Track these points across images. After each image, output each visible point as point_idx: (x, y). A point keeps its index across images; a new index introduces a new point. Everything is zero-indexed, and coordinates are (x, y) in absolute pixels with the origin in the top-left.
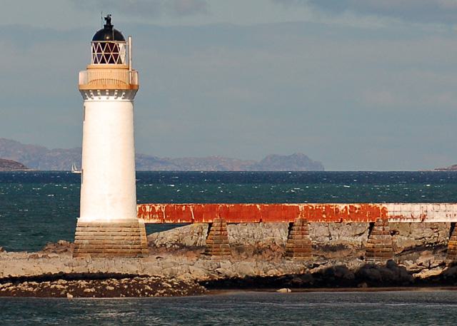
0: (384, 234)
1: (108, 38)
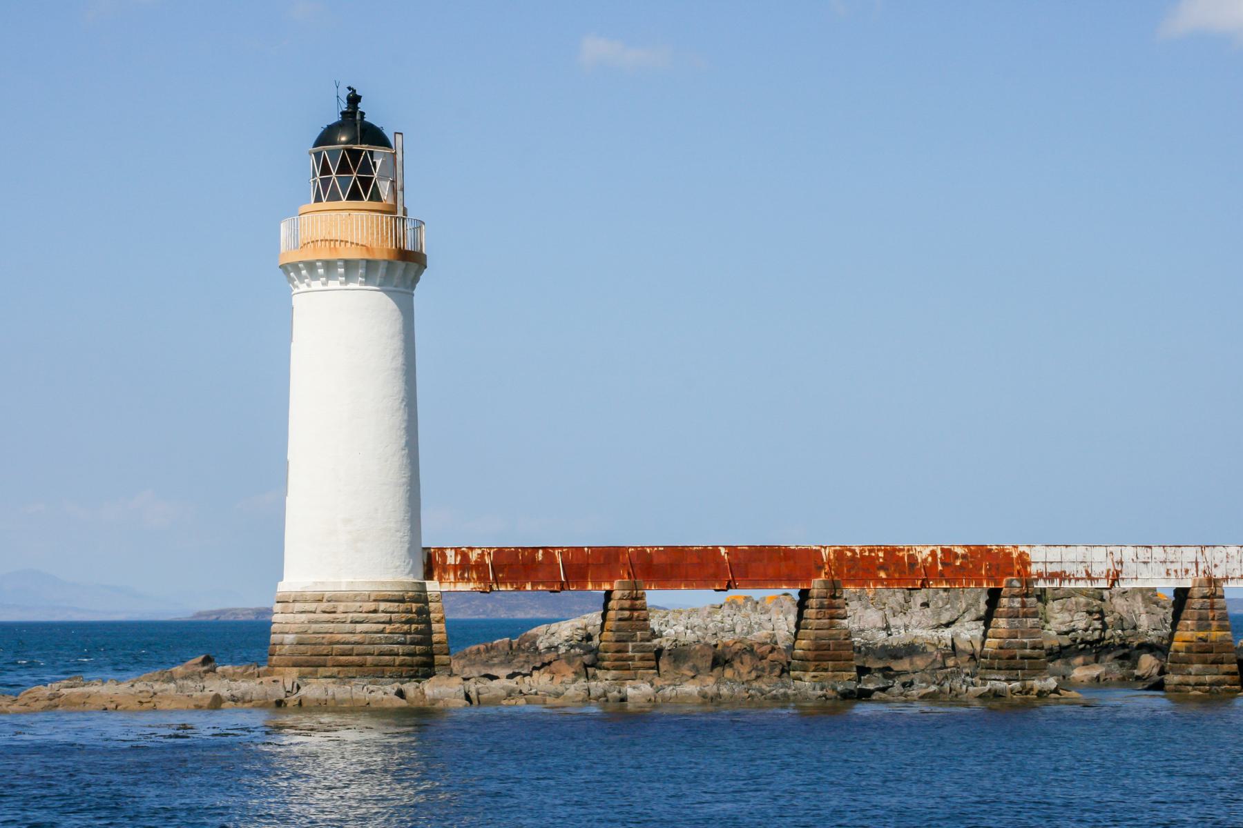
0: (1026, 616)
1: (343, 139)
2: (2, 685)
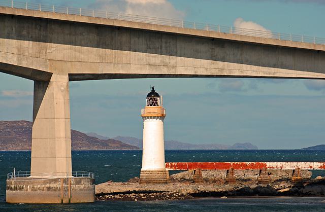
2: (324, 79)
